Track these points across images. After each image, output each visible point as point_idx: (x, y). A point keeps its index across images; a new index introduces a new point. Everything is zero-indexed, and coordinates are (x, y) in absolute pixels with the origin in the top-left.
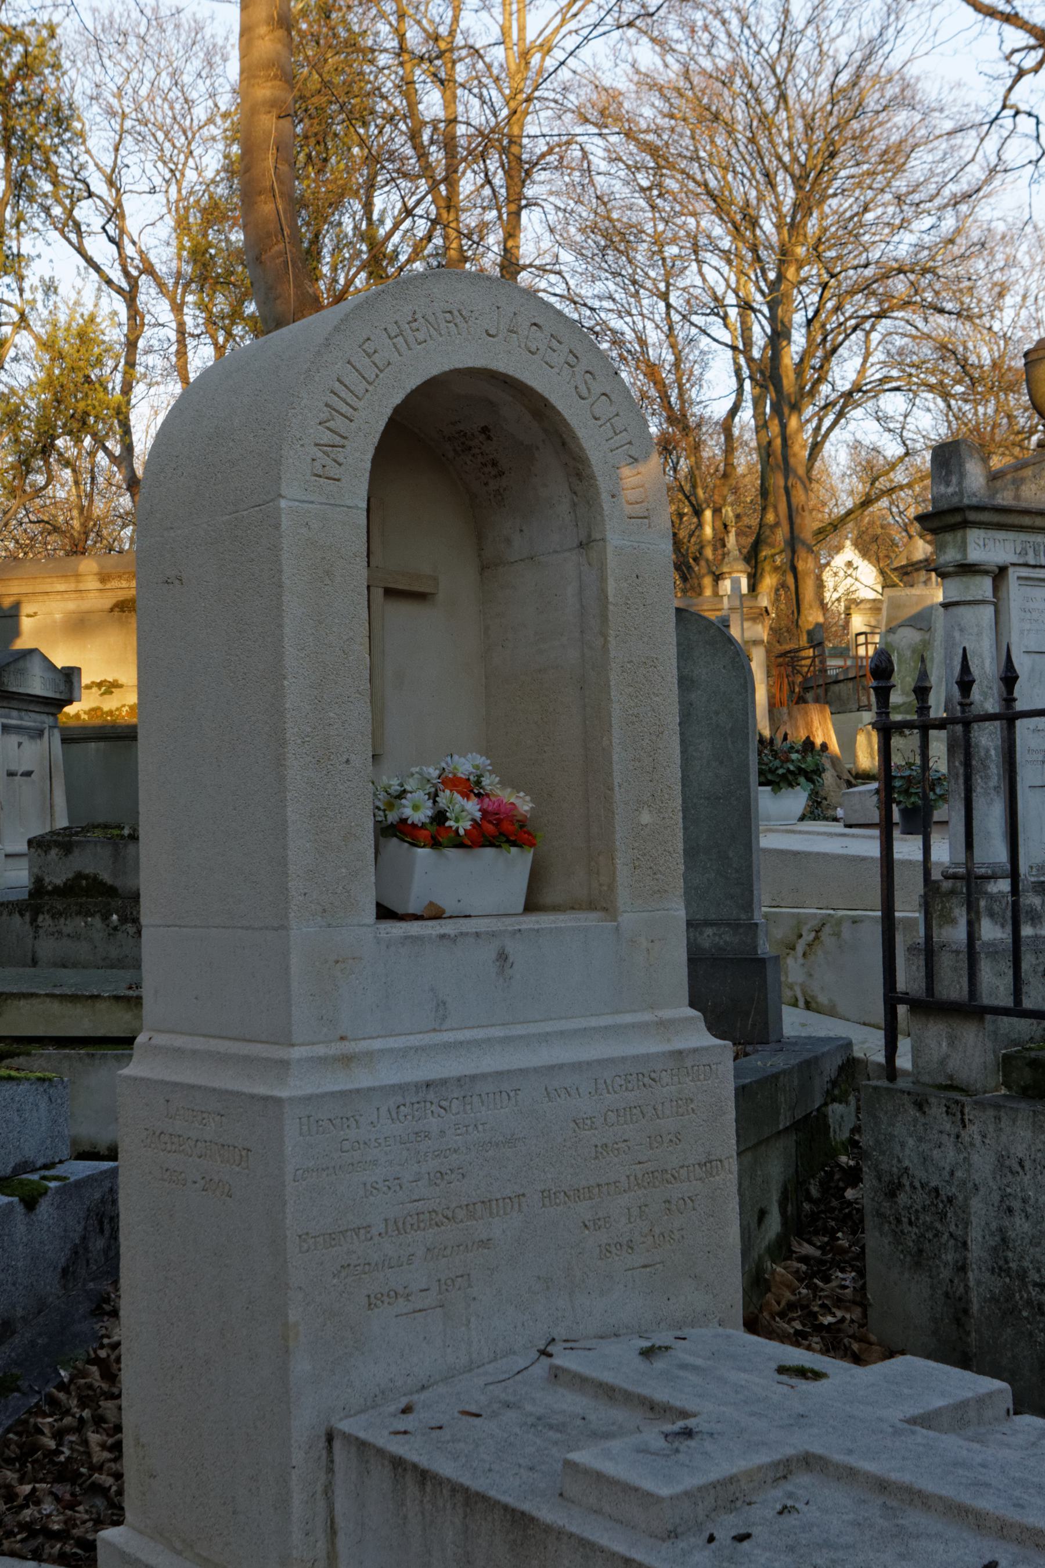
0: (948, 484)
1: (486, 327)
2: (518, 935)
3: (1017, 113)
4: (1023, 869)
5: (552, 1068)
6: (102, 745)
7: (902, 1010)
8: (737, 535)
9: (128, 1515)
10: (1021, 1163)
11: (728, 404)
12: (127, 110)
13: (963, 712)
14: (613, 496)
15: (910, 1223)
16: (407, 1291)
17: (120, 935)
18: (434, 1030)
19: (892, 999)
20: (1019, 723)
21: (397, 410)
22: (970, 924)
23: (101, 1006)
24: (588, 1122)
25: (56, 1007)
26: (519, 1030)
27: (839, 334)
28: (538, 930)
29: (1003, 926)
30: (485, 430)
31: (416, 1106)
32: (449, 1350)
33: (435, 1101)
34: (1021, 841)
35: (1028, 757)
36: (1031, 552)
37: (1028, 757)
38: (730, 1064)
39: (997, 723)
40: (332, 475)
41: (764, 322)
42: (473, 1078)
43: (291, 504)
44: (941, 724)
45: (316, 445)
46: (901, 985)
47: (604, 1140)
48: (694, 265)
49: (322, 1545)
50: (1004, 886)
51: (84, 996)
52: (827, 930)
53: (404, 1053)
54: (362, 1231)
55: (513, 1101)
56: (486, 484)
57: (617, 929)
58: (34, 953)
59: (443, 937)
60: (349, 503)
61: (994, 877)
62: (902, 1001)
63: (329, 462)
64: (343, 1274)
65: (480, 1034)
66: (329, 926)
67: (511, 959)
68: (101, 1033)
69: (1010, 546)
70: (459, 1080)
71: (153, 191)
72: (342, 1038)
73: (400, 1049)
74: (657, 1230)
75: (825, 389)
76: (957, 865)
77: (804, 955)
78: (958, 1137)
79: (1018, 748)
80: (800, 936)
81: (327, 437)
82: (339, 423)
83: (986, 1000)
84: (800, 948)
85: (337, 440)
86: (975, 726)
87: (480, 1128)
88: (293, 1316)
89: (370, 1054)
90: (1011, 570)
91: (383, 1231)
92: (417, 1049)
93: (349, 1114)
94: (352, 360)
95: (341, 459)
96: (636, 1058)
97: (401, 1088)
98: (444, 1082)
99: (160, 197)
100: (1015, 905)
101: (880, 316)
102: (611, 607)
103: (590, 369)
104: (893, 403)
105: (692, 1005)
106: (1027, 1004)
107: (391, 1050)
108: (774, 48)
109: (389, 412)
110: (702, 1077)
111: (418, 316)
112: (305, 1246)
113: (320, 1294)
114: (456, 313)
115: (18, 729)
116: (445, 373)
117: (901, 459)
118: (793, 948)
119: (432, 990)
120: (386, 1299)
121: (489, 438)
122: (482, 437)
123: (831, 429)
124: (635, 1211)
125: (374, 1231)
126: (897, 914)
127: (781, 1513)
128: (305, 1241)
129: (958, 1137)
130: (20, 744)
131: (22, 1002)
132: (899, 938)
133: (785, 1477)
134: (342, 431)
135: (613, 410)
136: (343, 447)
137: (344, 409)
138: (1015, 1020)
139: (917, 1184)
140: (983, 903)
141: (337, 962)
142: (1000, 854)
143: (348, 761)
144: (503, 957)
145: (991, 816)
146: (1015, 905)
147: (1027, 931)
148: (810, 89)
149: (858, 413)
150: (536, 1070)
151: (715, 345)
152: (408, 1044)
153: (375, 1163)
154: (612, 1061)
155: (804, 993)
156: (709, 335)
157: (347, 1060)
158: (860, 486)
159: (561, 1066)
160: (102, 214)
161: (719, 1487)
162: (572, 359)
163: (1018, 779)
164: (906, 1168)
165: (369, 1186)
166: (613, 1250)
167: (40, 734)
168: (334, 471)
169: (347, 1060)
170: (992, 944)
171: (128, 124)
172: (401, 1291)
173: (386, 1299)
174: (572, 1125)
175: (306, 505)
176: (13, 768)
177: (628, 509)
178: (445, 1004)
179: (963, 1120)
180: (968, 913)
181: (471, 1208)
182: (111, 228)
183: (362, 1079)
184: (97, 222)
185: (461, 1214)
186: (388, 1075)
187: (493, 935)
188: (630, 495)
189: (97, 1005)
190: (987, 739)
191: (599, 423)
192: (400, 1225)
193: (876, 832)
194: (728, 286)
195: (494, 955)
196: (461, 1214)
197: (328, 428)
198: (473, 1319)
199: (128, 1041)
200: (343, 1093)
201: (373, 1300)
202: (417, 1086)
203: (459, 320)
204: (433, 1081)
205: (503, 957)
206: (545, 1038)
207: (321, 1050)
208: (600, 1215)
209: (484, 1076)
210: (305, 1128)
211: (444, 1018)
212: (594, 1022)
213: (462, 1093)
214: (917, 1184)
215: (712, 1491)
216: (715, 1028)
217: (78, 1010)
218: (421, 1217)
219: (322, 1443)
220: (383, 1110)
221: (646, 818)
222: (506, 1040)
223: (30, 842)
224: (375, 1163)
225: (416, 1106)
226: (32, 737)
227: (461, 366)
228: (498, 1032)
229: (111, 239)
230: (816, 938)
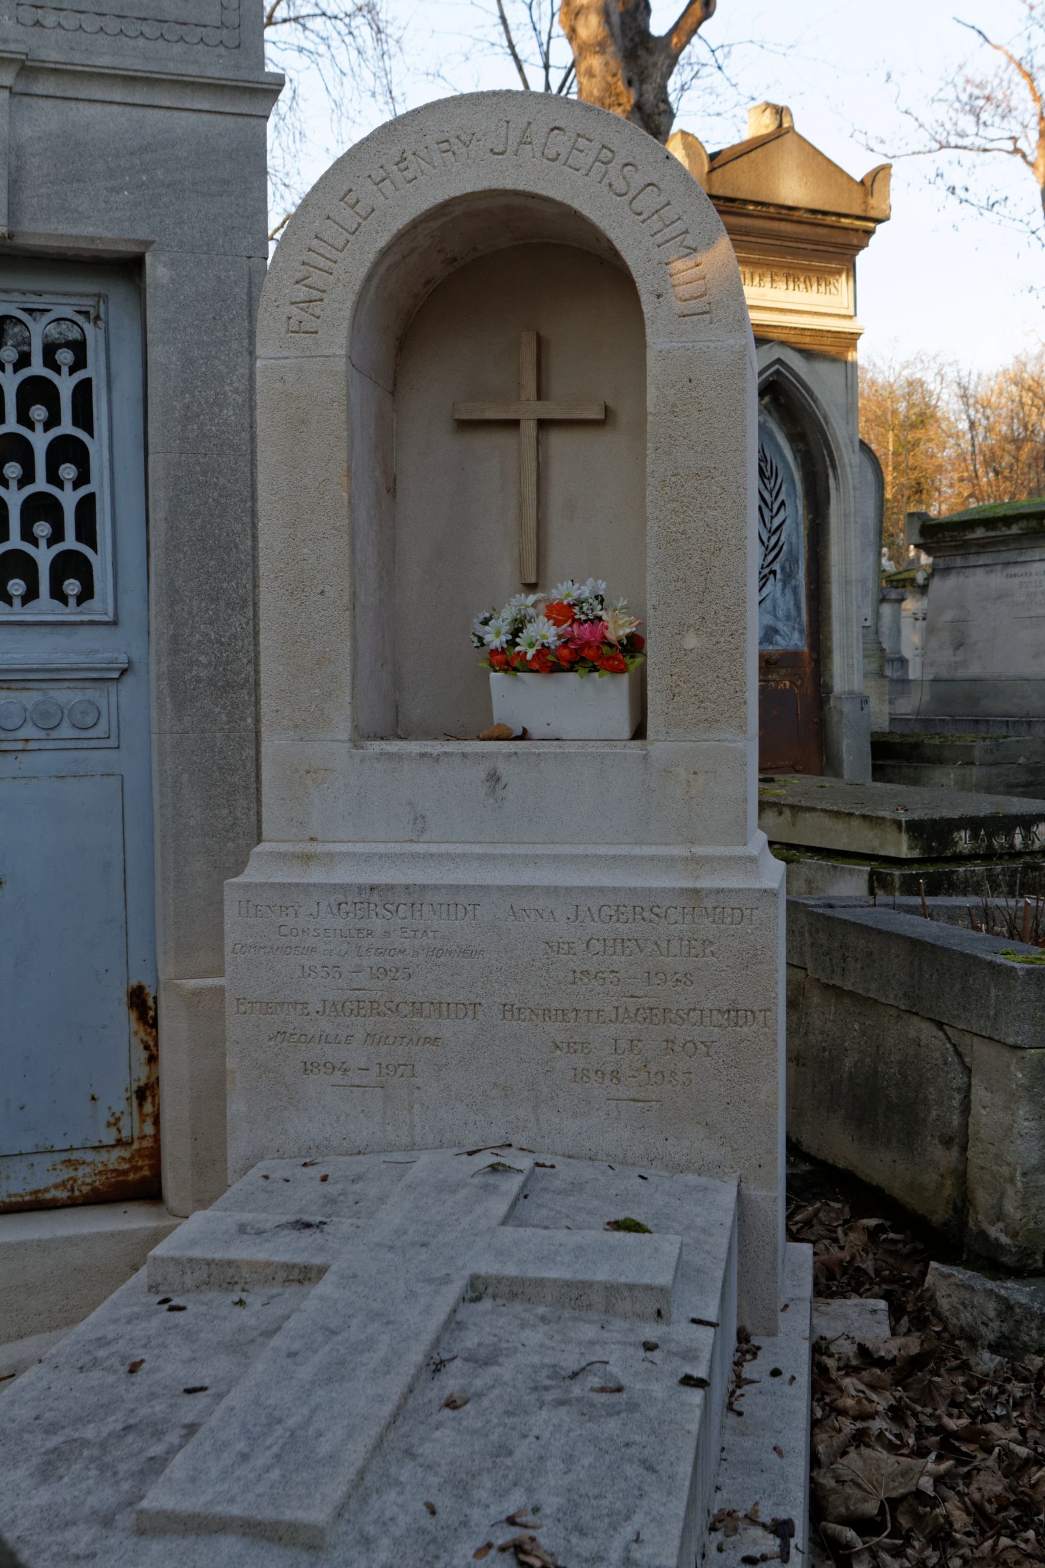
1: (490, 146)
2: (514, 758)
5: (520, 888)
14: (659, 296)
16: (344, 1066)
18: (411, 841)
23: (855, 823)
24: (566, 946)
25: (827, 822)
26: (508, 849)
28: (539, 754)
31: (359, 906)
32: (389, 1128)
33: (380, 903)
40: (308, 329)
42: (424, 887)
43: (265, 362)
45: (293, 303)
47: (585, 968)
51: (843, 813)
53: (368, 858)
54: (299, 1007)
55: (471, 914)
57: (645, 757)
59: (423, 755)
60: (327, 352)
63: (305, 316)
64: (279, 1039)
65: (459, 849)
66: (301, 739)
67: (504, 781)
68: (853, 848)
70: (407, 887)
72: (312, 839)
73: (362, 854)
74: (653, 1068)
81: (303, 293)
82: (316, 278)
85: (316, 294)
87: (431, 934)
88: (231, 1063)
89: (331, 856)
91: (320, 1009)
92: (381, 856)
93: (288, 904)
94: (331, 215)
95: (318, 312)
96: (633, 890)
97: (344, 888)
98: (390, 888)
102: (650, 418)
103: (630, 160)
107: (354, 854)
110: (728, 920)
111: (408, 154)
112: (243, 1008)
113: (256, 1051)
114: (453, 140)
119: (410, 803)
120: (323, 1069)
124: (623, 1044)
125: (310, 1008)
127: (236, 1304)
128: (242, 1004)
131: (807, 815)
133: (300, 1281)
134: (321, 285)
135: (663, 199)
136: (321, 300)
137: (322, 263)
141: (308, 772)
143: (322, 592)
144: (494, 778)
150: (500, 888)
152: (375, 851)
153: (313, 950)
154: (601, 890)
157: (307, 858)
159: (531, 889)
161: (213, 1266)
165: (306, 969)
168: (310, 324)
169: (307, 858)
172: (338, 1065)
173: (323, 1069)
174: (544, 946)
175: (282, 361)
177: (680, 307)
178: (423, 817)
181: (417, 1006)
183: (317, 875)
185: (405, 1009)
186: (342, 875)
187: (483, 756)
188: (684, 291)
189: (852, 823)
191: (641, 218)
192: (339, 1007)
195: (483, 776)
196: (405, 1009)
197: (306, 286)
198: (416, 1106)
200: (282, 885)
201: (309, 1066)
202: (360, 888)
203: (457, 146)
204: (378, 886)
205: (494, 778)
206: (535, 860)
207: (284, 847)
208: (577, 1039)
209: (436, 888)
210: (244, 910)
211: (423, 830)
212: (602, 850)
213: (411, 900)
215: (205, 1267)
217: (839, 825)
218: (362, 1005)
220: (323, 907)
221: (691, 641)
222: (482, 858)
224: (313, 950)
225: (359, 906)
227: (458, 194)
228: (477, 849)
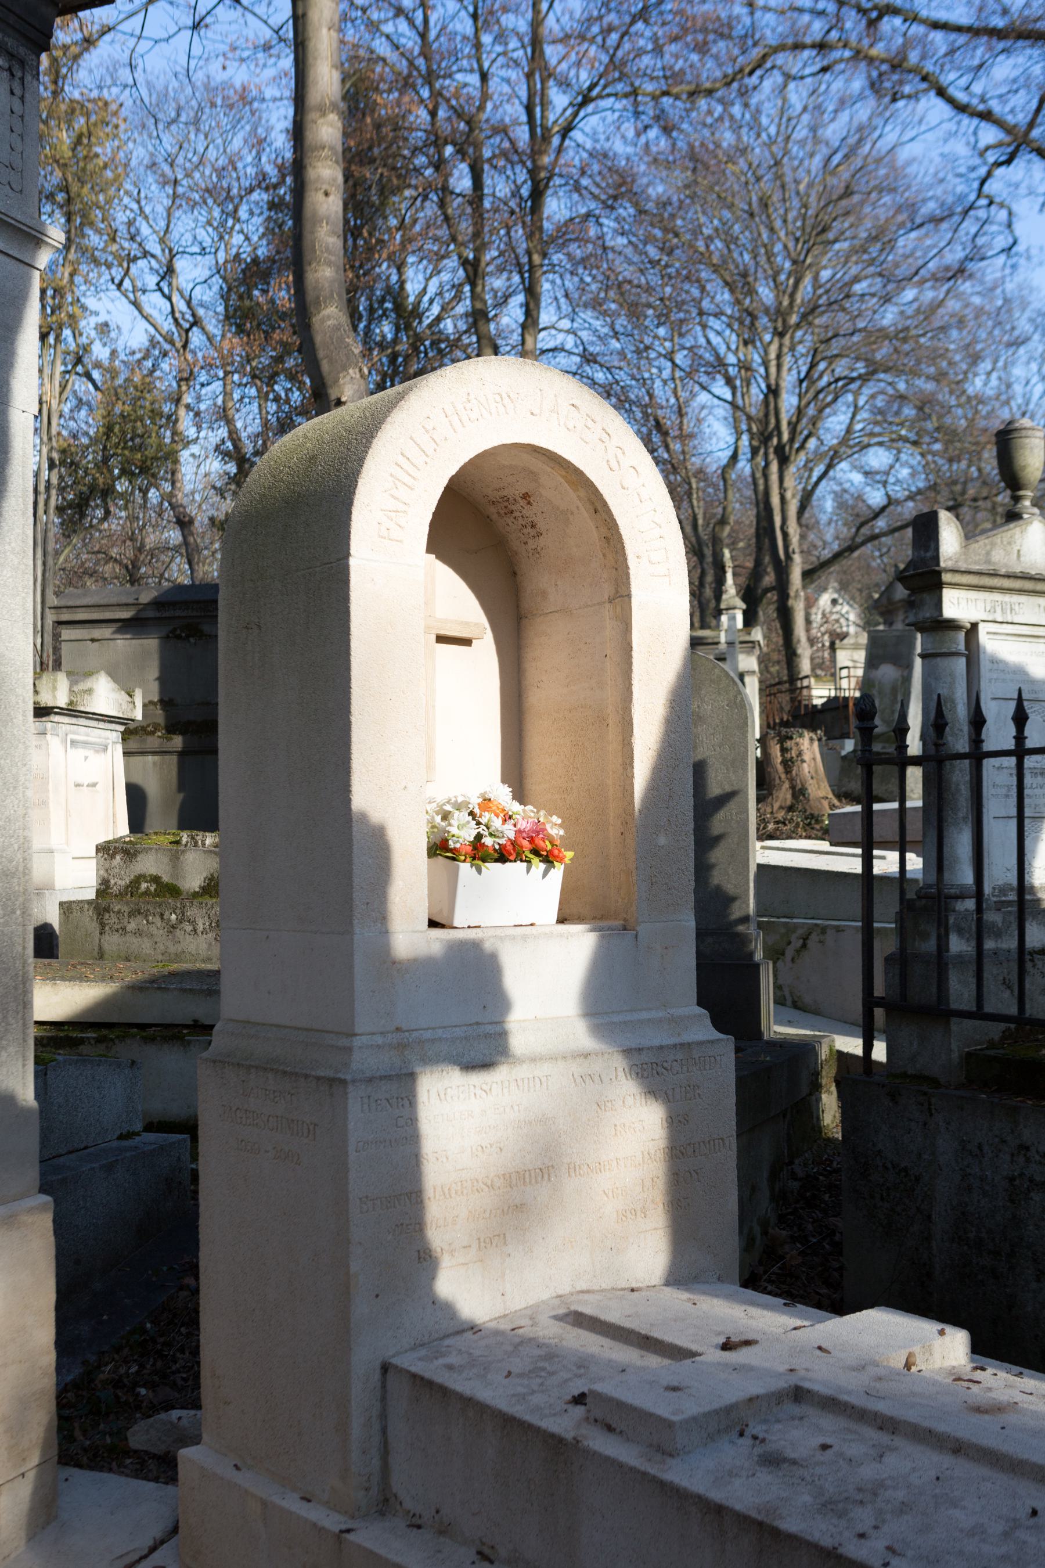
0: (927, 551)
3: (991, 203)
4: (987, 889)
6: (156, 758)
7: (879, 1013)
8: (734, 575)
9: (205, 1436)
10: (980, 1147)
11: (725, 456)
12: (179, 177)
13: (937, 751)
15: (882, 1199)
17: (178, 932)
19: (870, 1003)
20: (985, 761)
21: (452, 480)
22: (939, 937)
27: (829, 393)
29: (968, 940)
30: (526, 496)
34: (986, 866)
35: (993, 791)
36: (999, 609)
37: (993, 791)
38: (733, 1055)
39: (967, 762)
41: (760, 380)
44: (915, 761)
46: (879, 991)
48: (698, 328)
49: (376, 1462)
50: (970, 904)
52: (814, 937)
56: (526, 543)
58: (100, 948)
61: (962, 897)
62: (879, 1005)
69: (981, 605)
71: (203, 252)
75: (812, 443)
76: (930, 886)
77: (793, 960)
78: (925, 1124)
79: (985, 784)
80: (789, 943)
83: (954, 1006)
84: (790, 952)
86: (947, 763)
88: (354, 1267)
90: (981, 626)
99: (209, 260)
100: (979, 921)
101: (864, 379)
104: (878, 458)
105: (699, 1004)
106: (988, 1009)
108: (773, 130)
109: (445, 482)
115: (85, 744)
116: (495, 448)
117: (883, 509)
118: (783, 954)
121: (529, 503)
122: (523, 502)
123: (820, 479)
126: (876, 925)
129: (925, 1124)
130: (86, 758)
132: (877, 945)
138: (977, 1023)
139: (889, 1166)
140: (951, 921)
142: (966, 876)
145: (962, 843)
146: (979, 921)
147: (989, 944)
148: (807, 167)
149: (844, 465)
151: (716, 401)
155: (791, 993)
156: (709, 392)
158: (845, 530)
160: (157, 272)
162: (605, 437)
163: (985, 810)
164: (880, 1151)
166: (629, 1215)
167: (105, 749)
170: (960, 956)
171: (180, 190)
176: (80, 782)
179: (930, 1109)
180: (938, 929)
182: (164, 285)
184: (151, 281)
190: (960, 774)
193: (859, 851)
194: (729, 348)
199: (207, 1029)
203: (506, 401)
214: (889, 1166)
216: (719, 1024)
219: (377, 1375)
223: (98, 849)
226: (97, 751)
229: (164, 295)
230: (804, 946)
